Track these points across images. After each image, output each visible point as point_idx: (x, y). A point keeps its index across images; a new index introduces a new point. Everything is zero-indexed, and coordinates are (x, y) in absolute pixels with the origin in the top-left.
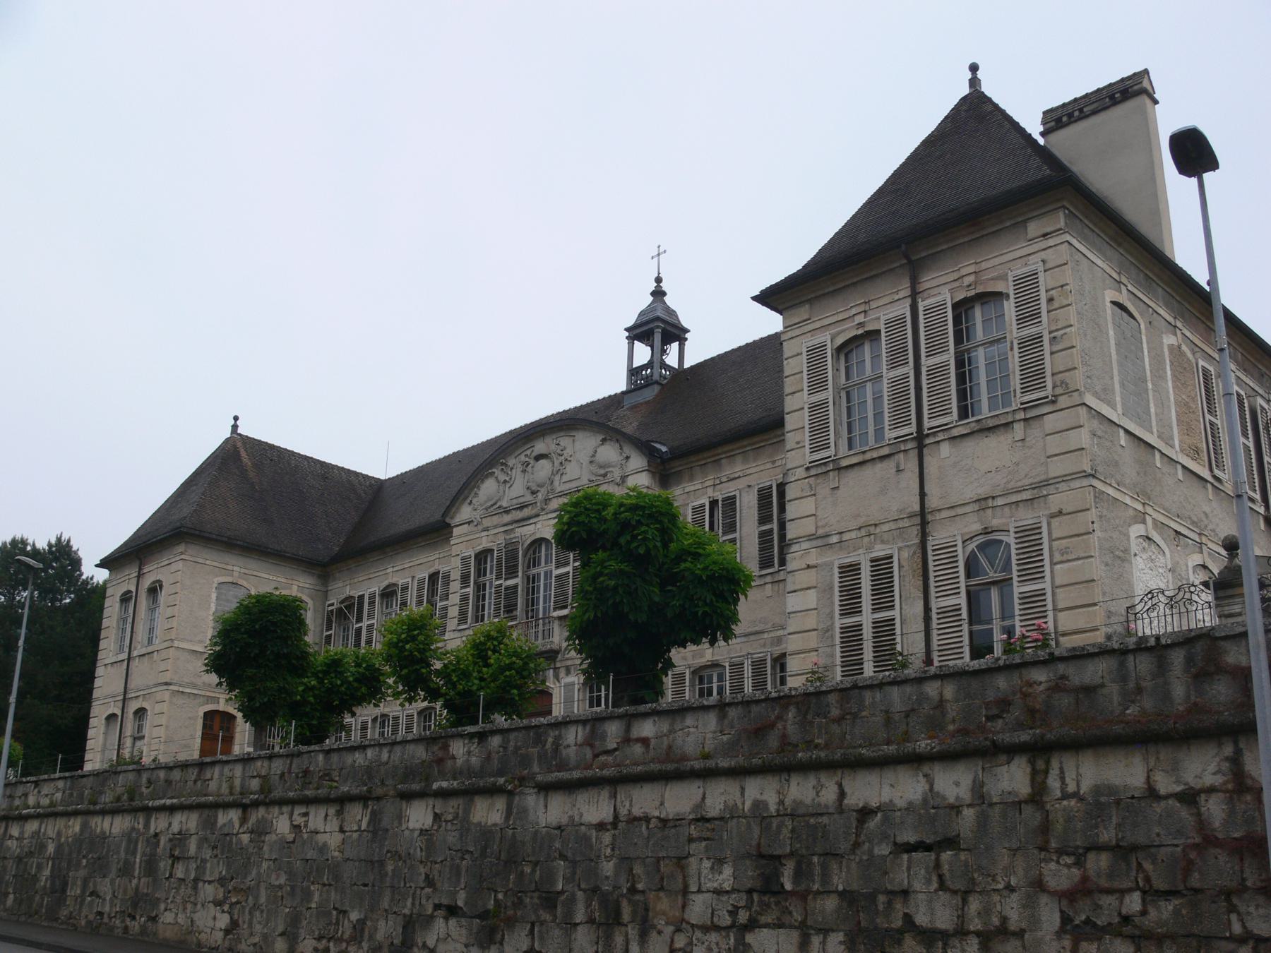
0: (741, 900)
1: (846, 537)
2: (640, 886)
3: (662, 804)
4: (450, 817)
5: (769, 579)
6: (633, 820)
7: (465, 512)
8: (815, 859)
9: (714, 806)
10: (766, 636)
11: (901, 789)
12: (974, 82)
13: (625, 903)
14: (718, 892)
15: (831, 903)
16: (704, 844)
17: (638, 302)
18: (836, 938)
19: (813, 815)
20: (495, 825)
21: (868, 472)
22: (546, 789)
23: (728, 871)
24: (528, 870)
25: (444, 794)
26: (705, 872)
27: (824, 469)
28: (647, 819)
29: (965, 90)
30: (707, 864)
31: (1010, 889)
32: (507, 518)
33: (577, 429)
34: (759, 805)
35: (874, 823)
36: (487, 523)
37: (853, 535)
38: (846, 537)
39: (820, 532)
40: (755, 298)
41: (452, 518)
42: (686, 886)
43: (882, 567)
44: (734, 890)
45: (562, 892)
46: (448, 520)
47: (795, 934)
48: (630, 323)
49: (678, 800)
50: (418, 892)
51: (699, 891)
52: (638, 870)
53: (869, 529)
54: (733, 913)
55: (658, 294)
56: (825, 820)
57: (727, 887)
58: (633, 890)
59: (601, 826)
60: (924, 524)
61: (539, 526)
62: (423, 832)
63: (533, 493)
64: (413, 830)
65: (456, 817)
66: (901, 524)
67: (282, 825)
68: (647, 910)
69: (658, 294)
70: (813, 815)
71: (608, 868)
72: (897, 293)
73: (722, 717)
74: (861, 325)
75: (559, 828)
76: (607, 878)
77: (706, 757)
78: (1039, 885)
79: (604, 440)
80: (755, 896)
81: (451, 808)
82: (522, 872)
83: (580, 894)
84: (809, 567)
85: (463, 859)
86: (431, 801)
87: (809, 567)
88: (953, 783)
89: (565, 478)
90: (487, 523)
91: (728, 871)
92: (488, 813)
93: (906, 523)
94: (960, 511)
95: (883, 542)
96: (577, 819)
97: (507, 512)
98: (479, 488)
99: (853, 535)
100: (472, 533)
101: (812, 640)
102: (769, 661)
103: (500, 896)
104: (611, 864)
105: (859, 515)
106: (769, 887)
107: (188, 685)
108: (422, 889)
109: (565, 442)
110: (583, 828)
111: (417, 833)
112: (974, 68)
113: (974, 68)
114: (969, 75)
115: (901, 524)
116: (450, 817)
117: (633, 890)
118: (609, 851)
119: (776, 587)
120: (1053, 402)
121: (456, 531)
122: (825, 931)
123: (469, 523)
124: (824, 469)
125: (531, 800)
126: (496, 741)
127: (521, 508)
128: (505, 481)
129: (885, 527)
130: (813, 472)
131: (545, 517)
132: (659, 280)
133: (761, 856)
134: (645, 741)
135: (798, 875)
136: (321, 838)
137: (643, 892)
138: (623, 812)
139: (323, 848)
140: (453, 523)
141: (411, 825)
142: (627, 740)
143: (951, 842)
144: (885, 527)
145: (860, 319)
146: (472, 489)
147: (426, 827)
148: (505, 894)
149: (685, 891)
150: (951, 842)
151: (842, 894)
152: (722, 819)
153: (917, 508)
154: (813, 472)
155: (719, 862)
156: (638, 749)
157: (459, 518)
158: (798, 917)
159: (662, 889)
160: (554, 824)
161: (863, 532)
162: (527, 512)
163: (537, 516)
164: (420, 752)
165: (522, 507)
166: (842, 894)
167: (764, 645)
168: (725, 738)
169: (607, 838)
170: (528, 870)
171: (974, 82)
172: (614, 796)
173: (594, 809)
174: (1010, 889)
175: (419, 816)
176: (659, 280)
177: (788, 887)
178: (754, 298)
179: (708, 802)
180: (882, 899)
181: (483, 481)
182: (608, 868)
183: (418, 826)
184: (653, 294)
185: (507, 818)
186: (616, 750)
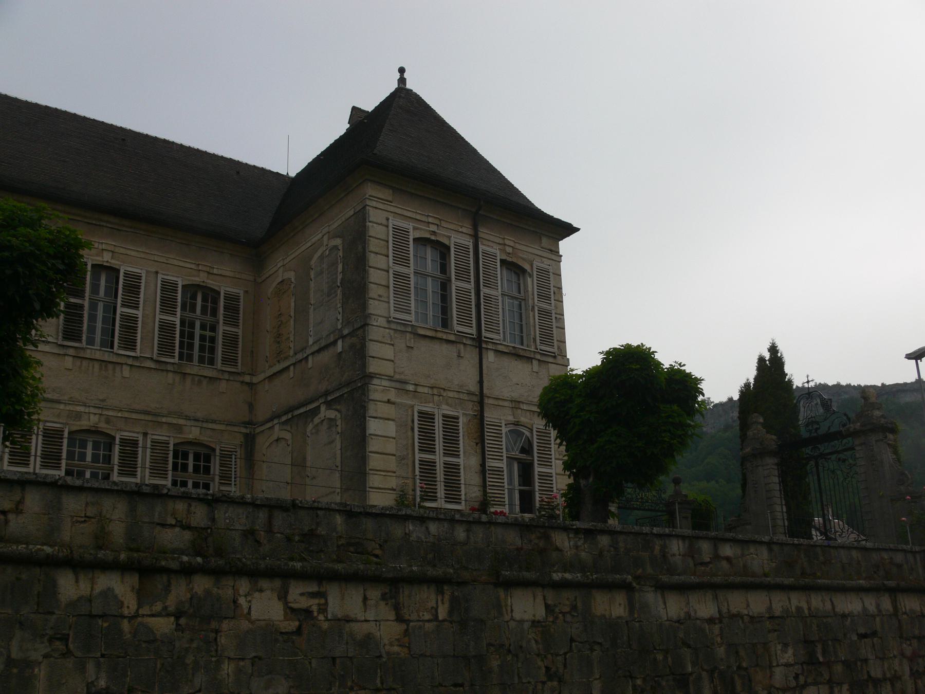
0: (797, 669)
1: (420, 389)
2: (744, 665)
3: (748, 606)
4: (567, 609)
5: (71, 352)
6: (733, 616)
8: (830, 643)
9: (778, 610)
10: (62, 407)
11: (851, 605)
12: (402, 81)
13: (736, 678)
14: (787, 665)
15: (839, 668)
16: (776, 633)
18: (845, 687)
19: (824, 617)
20: (619, 618)
21: (437, 347)
22: (663, 588)
23: (790, 651)
24: (660, 657)
25: (563, 585)
26: (779, 652)
27: (402, 328)
28: (739, 616)
29: (394, 85)
30: (779, 647)
31: (895, 657)
34: (799, 609)
35: (848, 622)
37: (426, 390)
38: (420, 389)
39: (397, 377)
40: (577, 230)
42: (771, 662)
43: (450, 422)
44: (796, 663)
45: (691, 674)
47: (827, 687)
49: (757, 603)
50: (540, 686)
51: (778, 665)
52: (742, 653)
53: (438, 390)
54: (796, 677)
56: (829, 620)
57: (791, 661)
58: (739, 667)
59: (711, 621)
60: (481, 403)
62: (535, 623)
64: (521, 622)
65: (574, 608)
66: (461, 396)
67: (265, 606)
68: (750, 681)
70: (824, 617)
71: (721, 651)
72: (461, 227)
73: (770, 550)
74: (434, 233)
75: (678, 621)
76: (722, 659)
77: (766, 575)
78: (903, 655)
80: (805, 666)
81: (567, 598)
82: (655, 659)
83: (704, 674)
84: (389, 402)
85: (592, 650)
86: (539, 592)
87: (389, 402)
88: (870, 603)
91: (790, 651)
92: (609, 606)
93: (465, 397)
94: (501, 403)
95: (447, 404)
96: (693, 614)
99: (426, 390)
101: (392, 463)
102: (66, 435)
103: (639, 682)
104: (722, 648)
105: (429, 376)
106: (811, 661)
108: (544, 683)
110: (698, 622)
111: (526, 625)
112: (402, 71)
113: (402, 71)
114: (398, 76)
115: (461, 396)
116: (567, 609)
117: (739, 667)
118: (719, 639)
119: (78, 362)
120: (555, 357)
122: (840, 684)
124: (402, 328)
125: (651, 597)
126: (604, 541)
129: (451, 394)
130: (393, 326)
133: (806, 642)
134: (728, 559)
135: (824, 652)
136: (359, 630)
137: (746, 669)
138: (725, 610)
139: (368, 641)
141: (517, 615)
142: (717, 557)
143: (874, 634)
144: (451, 394)
145: (433, 228)
147: (538, 618)
148: (644, 680)
149: (771, 667)
150: (874, 634)
151: (843, 662)
152: (782, 617)
153: (475, 388)
154: (393, 326)
155: (786, 645)
156: (724, 564)
158: (826, 676)
159: (757, 665)
160: (675, 618)
161: (435, 391)
164: (513, 538)
166: (843, 662)
167: (59, 416)
168: (774, 564)
169: (716, 629)
170: (660, 657)
171: (402, 81)
172: (716, 597)
173: (705, 607)
174: (895, 657)
175: (525, 607)
177: (821, 659)
178: (577, 230)
179: (774, 606)
180: (859, 663)
182: (721, 651)
183: (528, 616)
185: (631, 611)
186: (709, 563)
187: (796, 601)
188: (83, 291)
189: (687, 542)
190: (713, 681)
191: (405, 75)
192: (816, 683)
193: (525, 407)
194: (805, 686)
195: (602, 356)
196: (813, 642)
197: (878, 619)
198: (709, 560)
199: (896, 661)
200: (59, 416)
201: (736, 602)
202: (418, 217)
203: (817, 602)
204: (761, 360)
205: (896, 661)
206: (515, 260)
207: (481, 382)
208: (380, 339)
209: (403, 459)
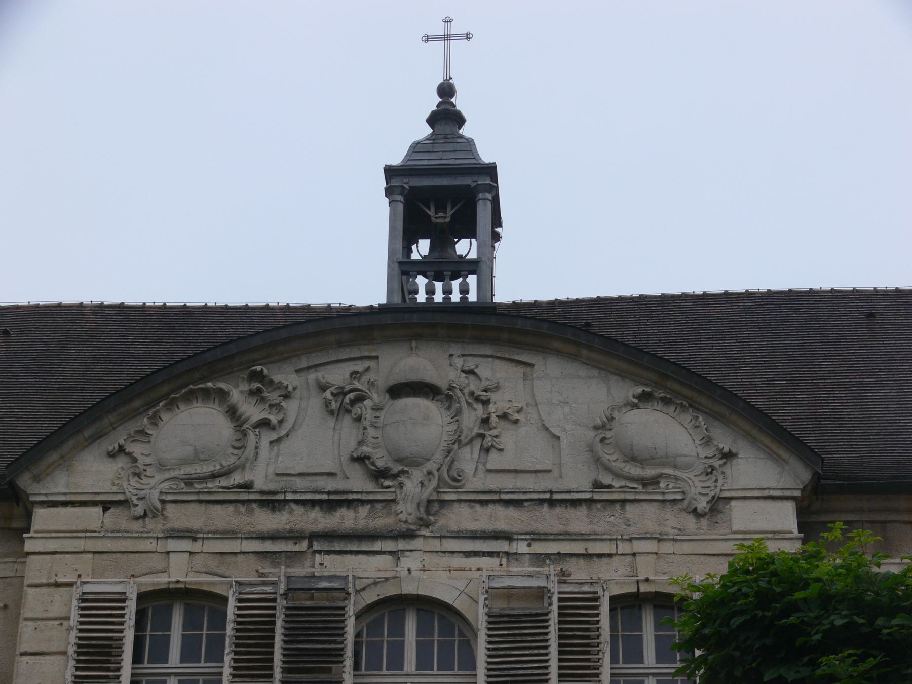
7: (93, 471)
17: (404, 130)
32: (267, 521)
33: (544, 349)
36: (178, 517)
41: (37, 479)
46: (25, 482)
48: (397, 159)
55: (446, 118)
61: (408, 562)
63: (379, 475)
69: (446, 118)
79: (645, 398)
89: (495, 460)
90: (178, 517)
97: (271, 502)
98: (155, 420)
100: (118, 533)
107: (208, 533)
109: (491, 370)
121: (42, 518)
123: (106, 506)
127: (331, 504)
128: (264, 424)
131: (436, 545)
132: (446, 90)
140: (36, 491)
146: (136, 414)
157: (58, 485)
162: (345, 519)
163: (409, 535)
165: (332, 503)
176: (446, 90)
181: (172, 405)
184: (432, 120)
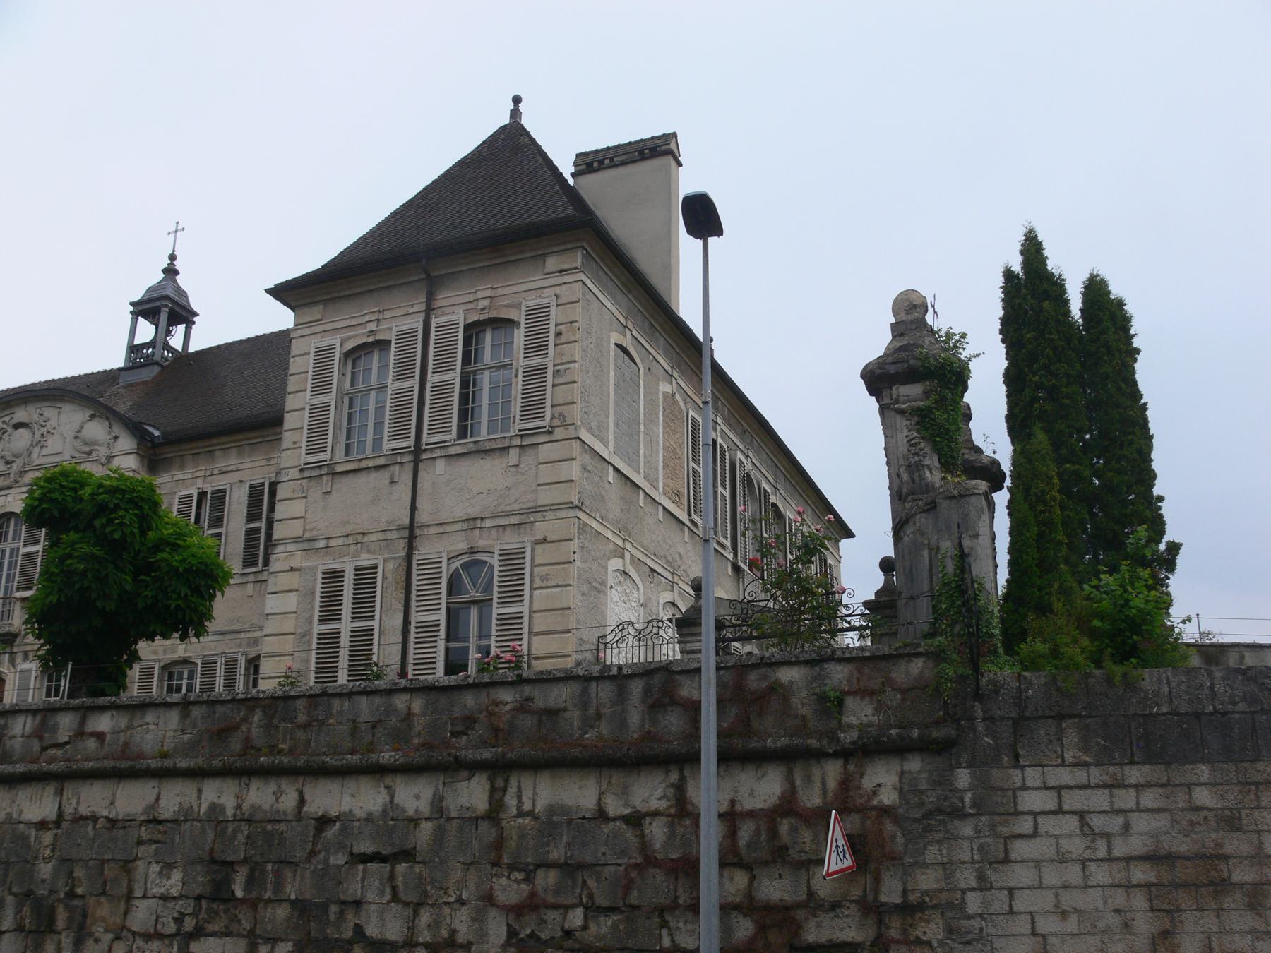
0: (188, 906)
1: (333, 543)
2: (79, 891)
5: (251, 578)
6: (79, 819)
8: (269, 866)
9: (168, 809)
10: (242, 635)
11: (364, 799)
12: (515, 113)
14: (165, 898)
16: (154, 847)
19: (270, 821)
23: (177, 876)
26: (152, 876)
27: (317, 473)
28: (94, 818)
30: (155, 868)
37: (340, 541)
39: (307, 535)
40: (269, 291)
42: (130, 891)
44: (181, 897)
49: (131, 799)
51: (145, 897)
52: (79, 873)
53: (357, 537)
54: (179, 921)
56: (283, 827)
57: (174, 892)
58: (71, 895)
59: (42, 825)
60: (411, 538)
66: (389, 536)
68: (85, 916)
70: (270, 821)
71: (45, 870)
72: (412, 306)
73: (185, 715)
74: (372, 333)
76: (43, 881)
78: (489, 899)
80: (204, 904)
84: (292, 569)
87: (292, 569)
91: (177, 876)
94: (448, 528)
95: (369, 552)
99: (340, 541)
104: (50, 865)
106: (219, 894)
110: (21, 826)
112: (517, 100)
113: (517, 100)
115: (389, 536)
117: (71, 895)
118: (48, 852)
120: (550, 433)
122: (273, 941)
124: (317, 473)
129: (374, 537)
133: (213, 861)
134: (100, 736)
135: (250, 882)
137: (82, 897)
138: (69, 810)
142: (80, 734)
144: (374, 537)
149: (129, 897)
150: (407, 855)
152: (175, 821)
153: (407, 521)
154: (307, 474)
155: (168, 866)
159: (103, 893)
161: (351, 540)
166: (294, 903)
167: (240, 645)
168: (186, 737)
169: (48, 837)
171: (515, 113)
177: (239, 894)
179: (162, 803)
180: (334, 908)
182: (45, 870)
186: (67, 743)
187: (219, 795)
188: (261, 514)
189: (38, 718)
190: (20, 911)
191: (522, 107)
192: (227, 934)
193: (488, 523)
194: (198, 933)
195: (1132, 332)
196: (231, 863)
197: (426, 827)
198: (66, 739)
199: (464, 914)
200: (240, 645)
201: (93, 799)
202: (354, 322)
203: (260, 795)
204: (1009, 274)
205: (464, 914)
206: (493, 314)
207: (413, 508)
208: (289, 496)
209: (305, 636)
